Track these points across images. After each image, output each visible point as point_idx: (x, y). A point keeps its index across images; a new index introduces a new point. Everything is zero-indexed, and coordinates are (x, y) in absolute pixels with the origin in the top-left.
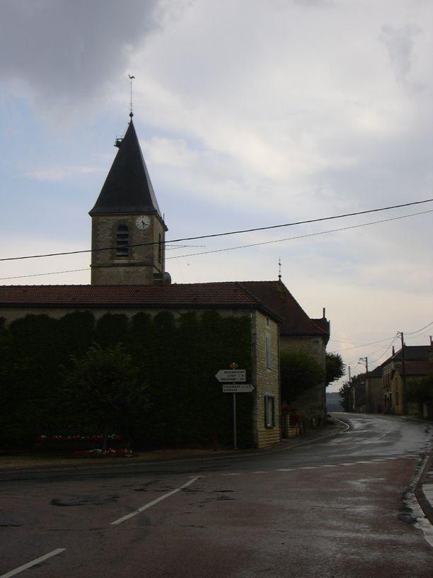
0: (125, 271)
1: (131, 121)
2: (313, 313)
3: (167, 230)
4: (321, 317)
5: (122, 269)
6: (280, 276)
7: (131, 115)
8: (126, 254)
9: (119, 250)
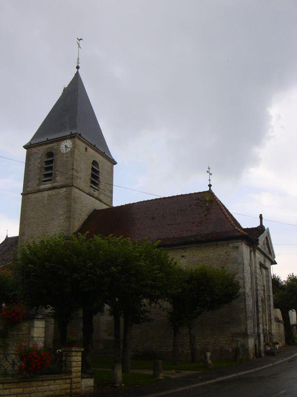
0: (49, 196)
1: (78, 72)
2: (247, 222)
3: (115, 163)
4: (207, 189)
5: (46, 193)
6: (210, 186)
7: (78, 68)
8: (50, 178)
9: (46, 176)
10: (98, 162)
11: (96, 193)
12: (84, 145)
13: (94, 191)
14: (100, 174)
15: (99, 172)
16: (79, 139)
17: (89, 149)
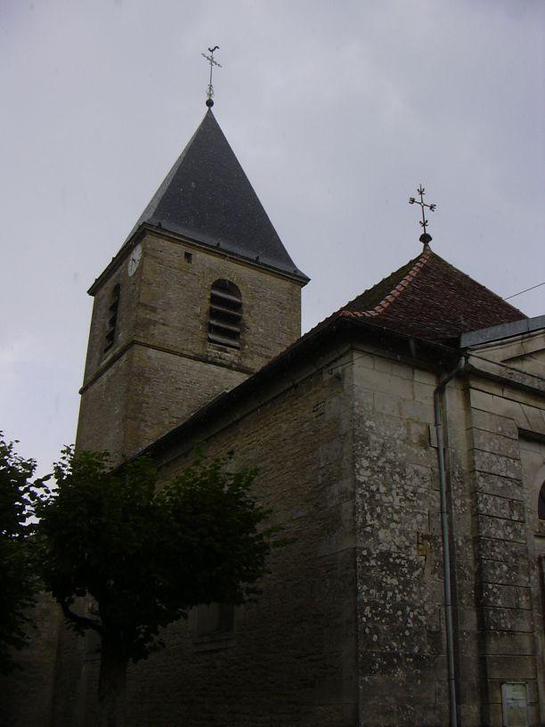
1: (210, 112)
3: (304, 280)
7: (210, 103)
10: (235, 281)
11: (230, 356)
12: (180, 249)
13: (220, 349)
14: (245, 309)
15: (238, 306)
16: (160, 236)
17: (198, 256)
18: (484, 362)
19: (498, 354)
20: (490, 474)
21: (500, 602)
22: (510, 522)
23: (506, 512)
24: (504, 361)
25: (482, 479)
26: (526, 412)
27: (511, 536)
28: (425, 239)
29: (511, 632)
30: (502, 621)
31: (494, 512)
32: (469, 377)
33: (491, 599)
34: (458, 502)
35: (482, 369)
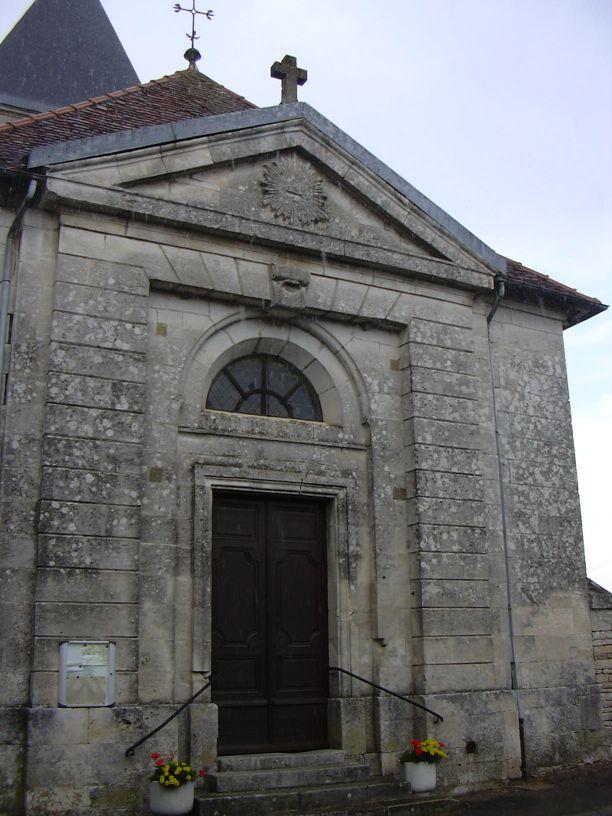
18: (77, 187)
19: (113, 174)
20: (80, 345)
21: (72, 527)
22: (110, 411)
23: (105, 399)
24: (122, 185)
25: (61, 353)
26: (170, 257)
27: (110, 433)
28: (192, 55)
29: (90, 571)
30: (74, 554)
31: (79, 398)
32: (57, 209)
33: (56, 523)
34: (20, 388)
35: (72, 197)
